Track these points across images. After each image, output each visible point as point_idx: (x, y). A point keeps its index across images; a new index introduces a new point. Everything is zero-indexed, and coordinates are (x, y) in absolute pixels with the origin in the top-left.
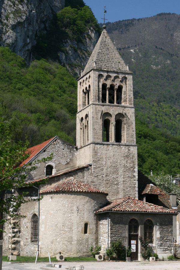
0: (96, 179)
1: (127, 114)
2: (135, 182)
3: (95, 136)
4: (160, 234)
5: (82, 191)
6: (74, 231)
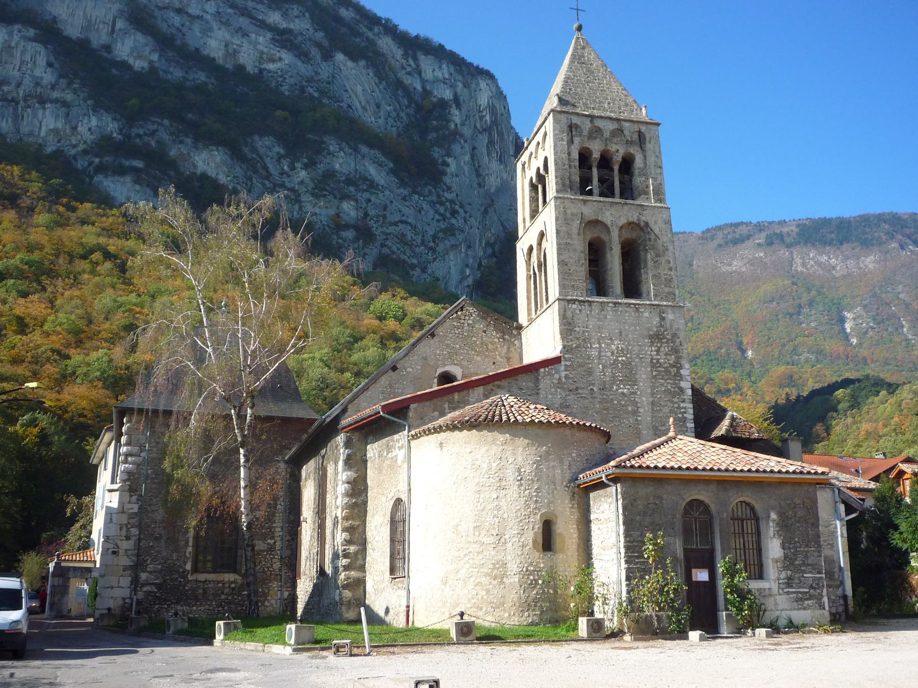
0: (571, 397)
1: (652, 225)
2: (682, 405)
3: (566, 282)
4: (784, 548)
5: (532, 421)
6: (509, 545)
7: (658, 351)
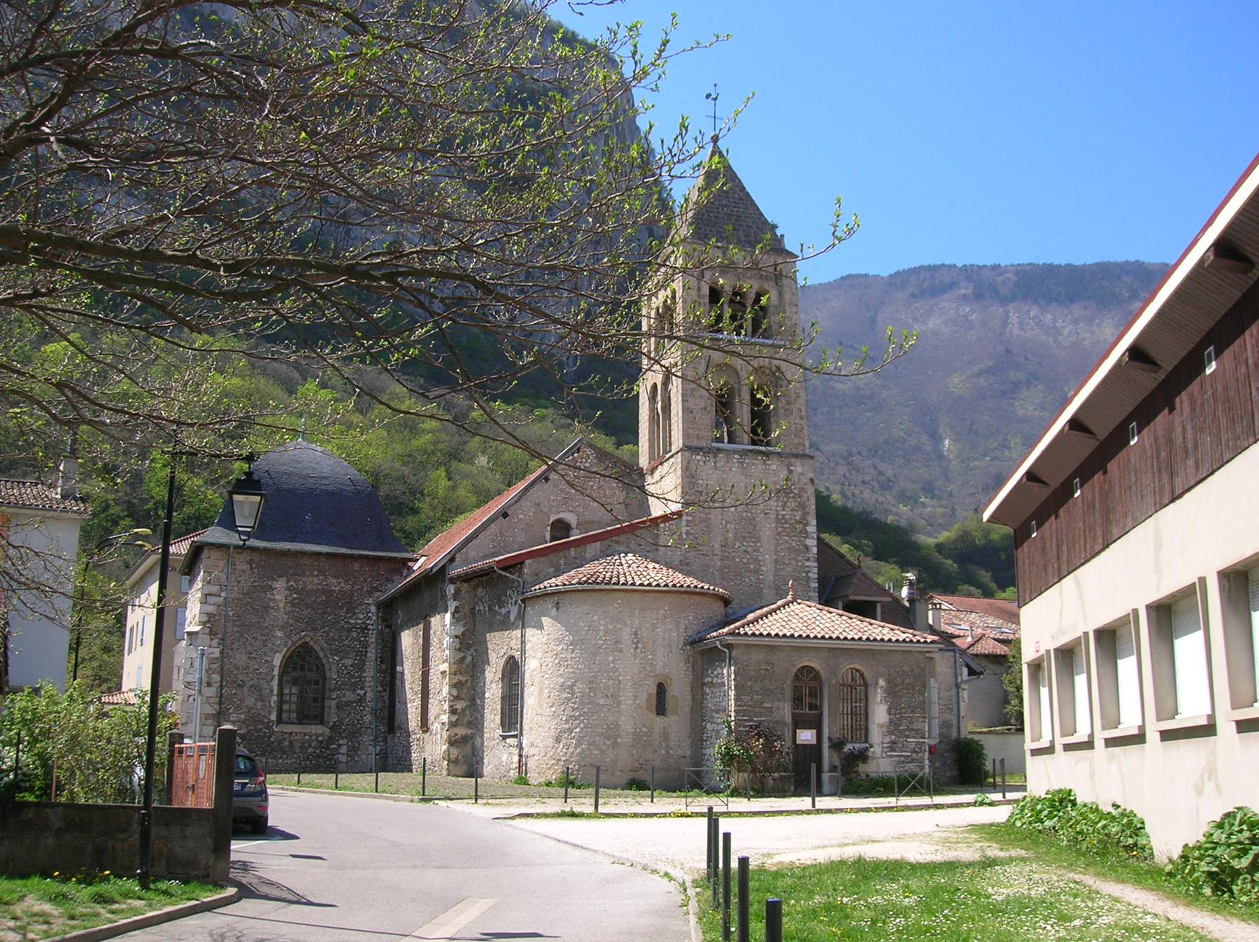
7: (784, 506)
